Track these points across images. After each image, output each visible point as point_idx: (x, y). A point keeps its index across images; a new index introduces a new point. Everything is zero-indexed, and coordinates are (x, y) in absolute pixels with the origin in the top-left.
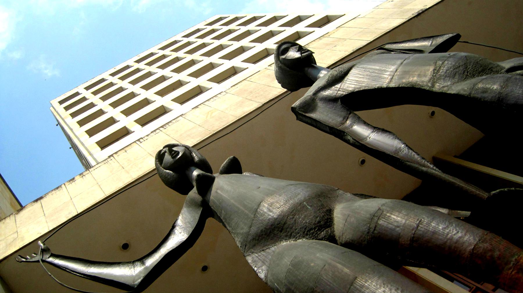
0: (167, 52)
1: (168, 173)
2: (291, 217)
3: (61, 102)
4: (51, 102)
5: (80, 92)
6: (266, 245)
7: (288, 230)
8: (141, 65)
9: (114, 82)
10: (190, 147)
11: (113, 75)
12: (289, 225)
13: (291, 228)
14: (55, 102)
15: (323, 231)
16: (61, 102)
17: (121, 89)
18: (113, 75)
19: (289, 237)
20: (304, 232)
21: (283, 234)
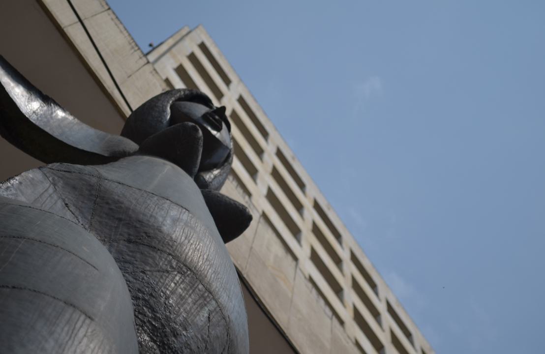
0: (350, 268)
1: (164, 111)
2: (174, 264)
3: (203, 47)
4: (201, 27)
5: (232, 86)
6: (81, 212)
7: (138, 255)
8: (311, 214)
9: (266, 156)
10: (230, 164)
11: (280, 154)
12: (153, 258)
13: (147, 264)
14: (201, 36)
15: (152, 340)
16: (203, 47)
17: (259, 152)
18: (280, 154)
19: (122, 262)
20: (139, 290)
21: (123, 246)
